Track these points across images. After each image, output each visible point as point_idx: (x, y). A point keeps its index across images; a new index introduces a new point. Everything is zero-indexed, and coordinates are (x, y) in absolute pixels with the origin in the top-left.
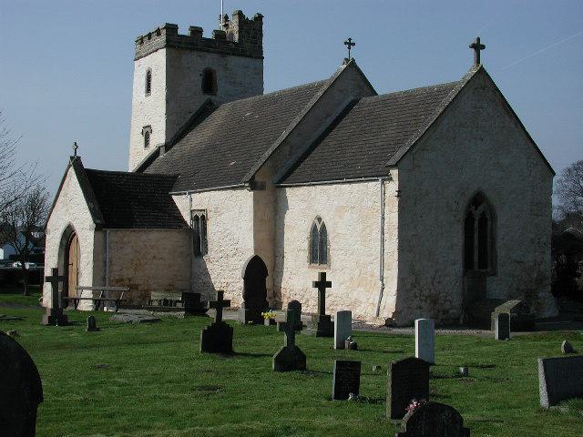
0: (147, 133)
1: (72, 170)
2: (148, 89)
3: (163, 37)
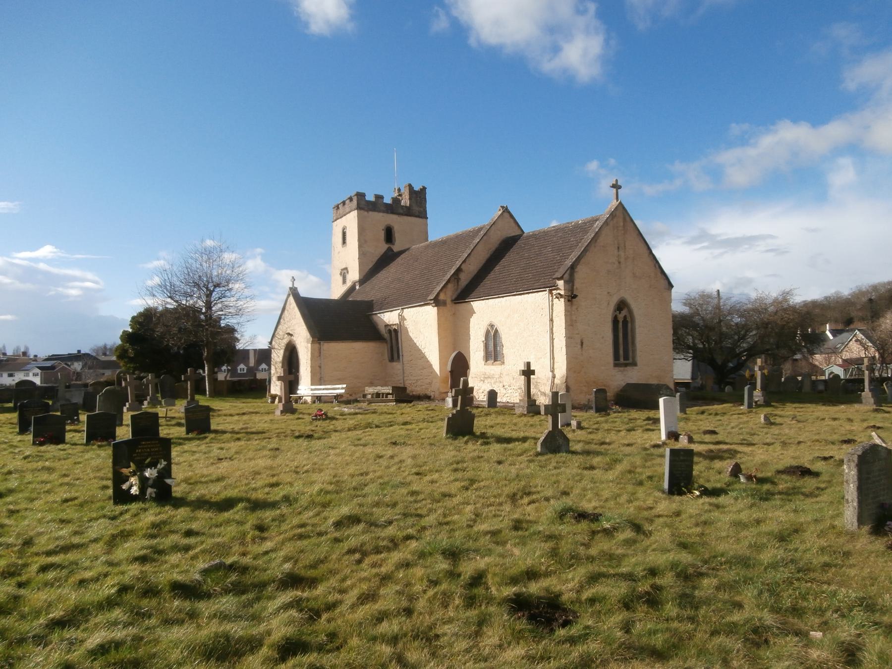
0: (344, 272)
2: (344, 242)
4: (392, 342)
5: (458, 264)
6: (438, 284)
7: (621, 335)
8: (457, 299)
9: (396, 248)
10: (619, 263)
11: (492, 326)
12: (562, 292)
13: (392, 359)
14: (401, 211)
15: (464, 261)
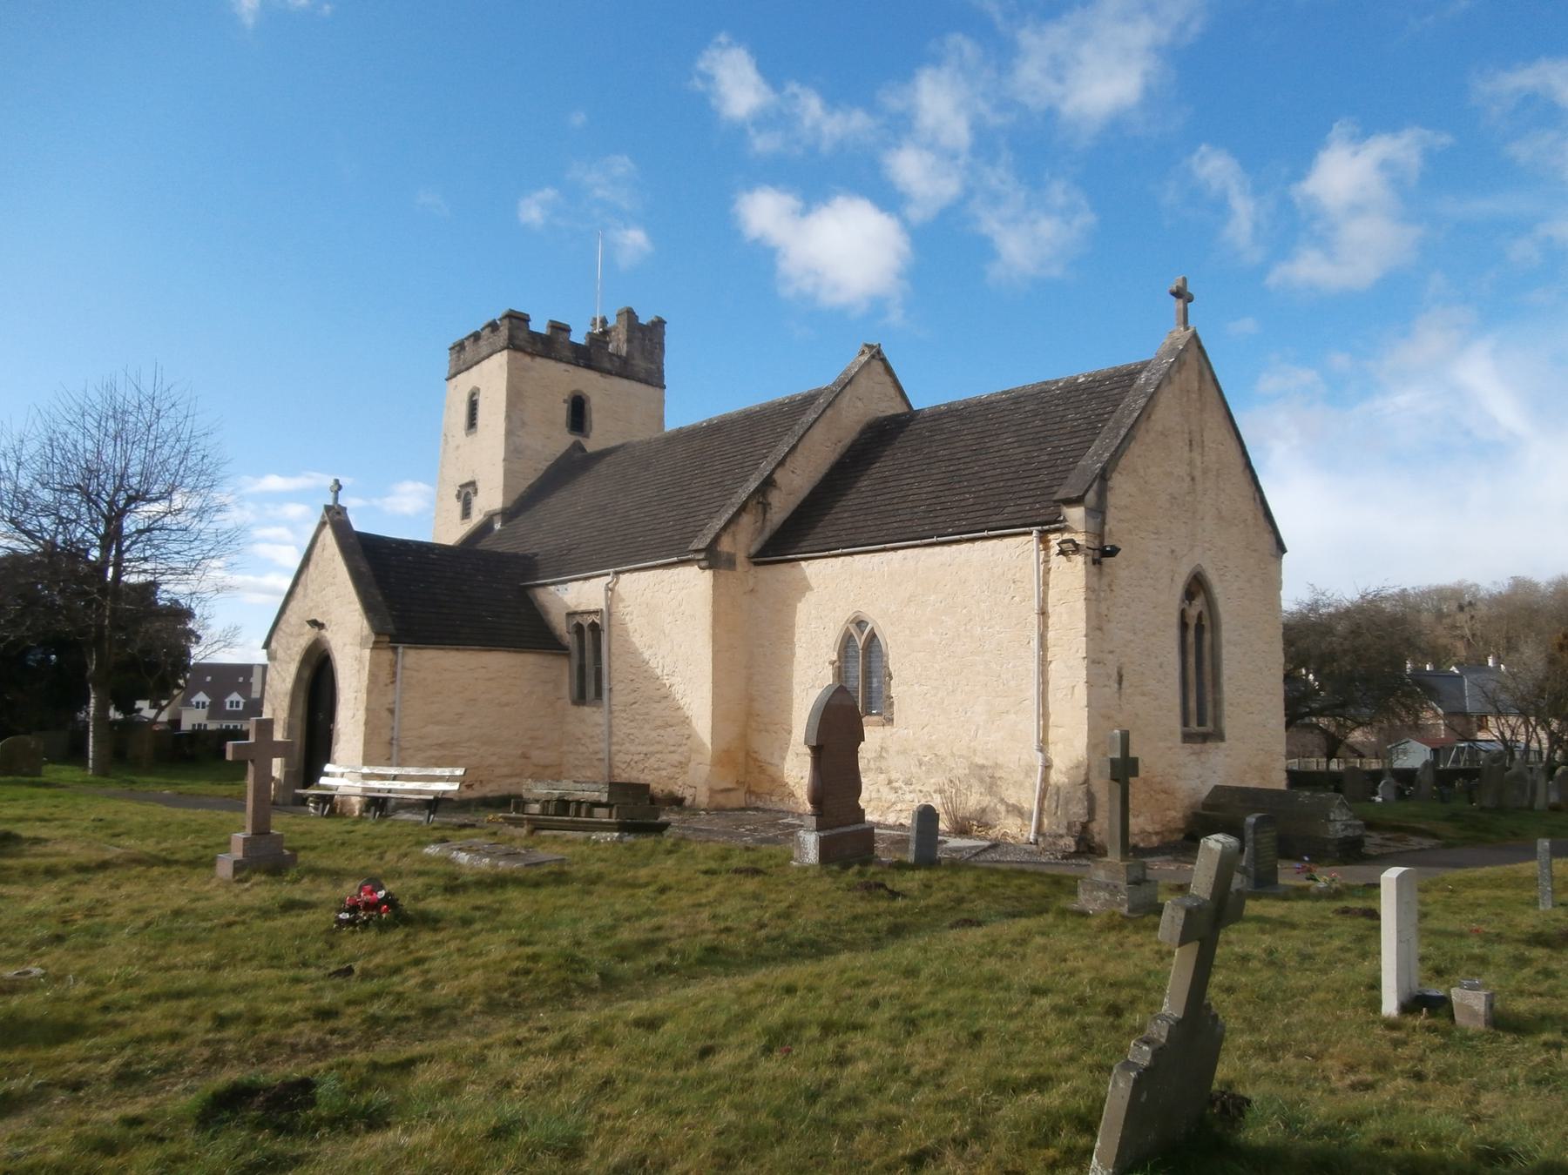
0: (466, 493)
1: (328, 535)
3: (504, 332)
4: (585, 654)
5: (765, 468)
6: (710, 516)
7: (1192, 660)
8: (762, 552)
9: (593, 444)
10: (1193, 479)
11: (860, 623)
12: (1080, 539)
13: (580, 699)
14: (608, 366)
15: (781, 463)
